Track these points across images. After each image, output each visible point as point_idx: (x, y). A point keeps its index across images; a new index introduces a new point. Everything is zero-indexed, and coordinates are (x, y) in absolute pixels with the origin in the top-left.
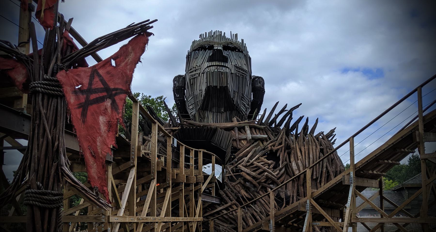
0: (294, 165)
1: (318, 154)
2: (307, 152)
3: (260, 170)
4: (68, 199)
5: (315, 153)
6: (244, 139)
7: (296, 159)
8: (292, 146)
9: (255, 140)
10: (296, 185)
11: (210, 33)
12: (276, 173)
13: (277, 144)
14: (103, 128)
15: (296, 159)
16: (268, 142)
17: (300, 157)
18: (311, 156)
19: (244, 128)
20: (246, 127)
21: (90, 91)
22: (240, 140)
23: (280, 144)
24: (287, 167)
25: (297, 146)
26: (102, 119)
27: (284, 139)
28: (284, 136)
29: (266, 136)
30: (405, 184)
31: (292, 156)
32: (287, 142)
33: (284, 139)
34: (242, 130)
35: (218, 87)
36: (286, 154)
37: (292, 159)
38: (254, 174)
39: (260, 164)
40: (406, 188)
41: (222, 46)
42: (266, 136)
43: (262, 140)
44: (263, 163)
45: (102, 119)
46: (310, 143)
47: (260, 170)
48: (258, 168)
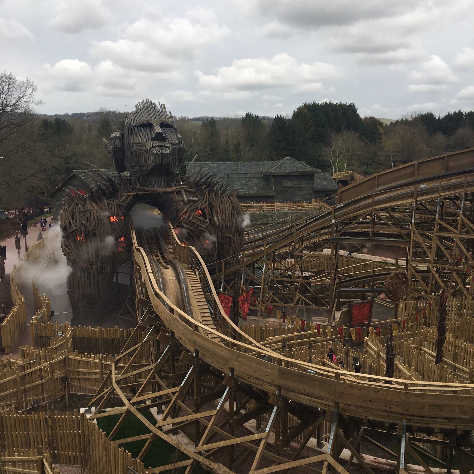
0: (215, 218)
1: (231, 210)
2: (224, 209)
3: (196, 225)
4: (128, 283)
5: (229, 210)
6: (181, 201)
7: (217, 214)
8: (213, 204)
9: (189, 201)
10: (216, 232)
11: (143, 102)
12: (205, 226)
13: (204, 203)
14: (246, 307)
15: (217, 214)
16: (198, 203)
17: (220, 213)
18: (227, 213)
19: (180, 192)
20: (182, 191)
21: (244, 301)
22: (179, 201)
23: (206, 202)
24: (211, 220)
25: (217, 205)
26: (246, 306)
27: (207, 199)
28: (208, 196)
29: (197, 199)
30: (271, 172)
31: (214, 212)
32: (209, 201)
33: (207, 199)
34: (179, 193)
35: (163, 165)
36: (209, 209)
37: (214, 214)
38: (192, 228)
39: (195, 221)
40: (272, 175)
41: (159, 124)
42: (197, 199)
43: (194, 201)
44: (196, 220)
45: (246, 306)
46: (226, 203)
47: (196, 225)
48: (194, 223)
